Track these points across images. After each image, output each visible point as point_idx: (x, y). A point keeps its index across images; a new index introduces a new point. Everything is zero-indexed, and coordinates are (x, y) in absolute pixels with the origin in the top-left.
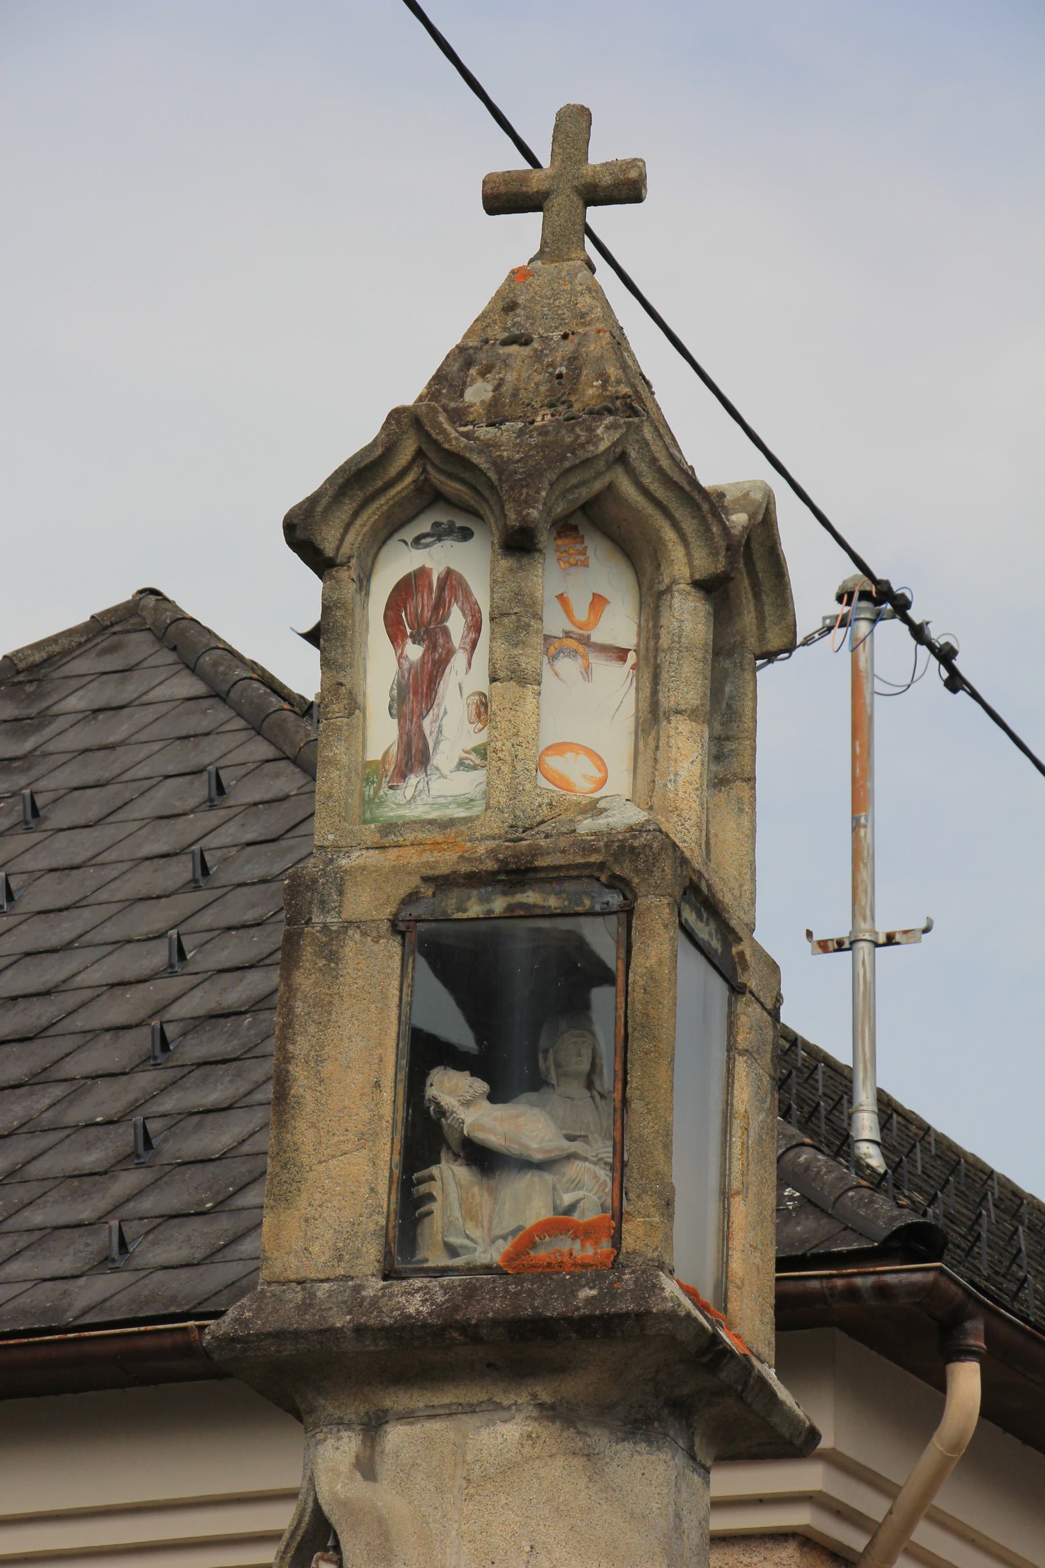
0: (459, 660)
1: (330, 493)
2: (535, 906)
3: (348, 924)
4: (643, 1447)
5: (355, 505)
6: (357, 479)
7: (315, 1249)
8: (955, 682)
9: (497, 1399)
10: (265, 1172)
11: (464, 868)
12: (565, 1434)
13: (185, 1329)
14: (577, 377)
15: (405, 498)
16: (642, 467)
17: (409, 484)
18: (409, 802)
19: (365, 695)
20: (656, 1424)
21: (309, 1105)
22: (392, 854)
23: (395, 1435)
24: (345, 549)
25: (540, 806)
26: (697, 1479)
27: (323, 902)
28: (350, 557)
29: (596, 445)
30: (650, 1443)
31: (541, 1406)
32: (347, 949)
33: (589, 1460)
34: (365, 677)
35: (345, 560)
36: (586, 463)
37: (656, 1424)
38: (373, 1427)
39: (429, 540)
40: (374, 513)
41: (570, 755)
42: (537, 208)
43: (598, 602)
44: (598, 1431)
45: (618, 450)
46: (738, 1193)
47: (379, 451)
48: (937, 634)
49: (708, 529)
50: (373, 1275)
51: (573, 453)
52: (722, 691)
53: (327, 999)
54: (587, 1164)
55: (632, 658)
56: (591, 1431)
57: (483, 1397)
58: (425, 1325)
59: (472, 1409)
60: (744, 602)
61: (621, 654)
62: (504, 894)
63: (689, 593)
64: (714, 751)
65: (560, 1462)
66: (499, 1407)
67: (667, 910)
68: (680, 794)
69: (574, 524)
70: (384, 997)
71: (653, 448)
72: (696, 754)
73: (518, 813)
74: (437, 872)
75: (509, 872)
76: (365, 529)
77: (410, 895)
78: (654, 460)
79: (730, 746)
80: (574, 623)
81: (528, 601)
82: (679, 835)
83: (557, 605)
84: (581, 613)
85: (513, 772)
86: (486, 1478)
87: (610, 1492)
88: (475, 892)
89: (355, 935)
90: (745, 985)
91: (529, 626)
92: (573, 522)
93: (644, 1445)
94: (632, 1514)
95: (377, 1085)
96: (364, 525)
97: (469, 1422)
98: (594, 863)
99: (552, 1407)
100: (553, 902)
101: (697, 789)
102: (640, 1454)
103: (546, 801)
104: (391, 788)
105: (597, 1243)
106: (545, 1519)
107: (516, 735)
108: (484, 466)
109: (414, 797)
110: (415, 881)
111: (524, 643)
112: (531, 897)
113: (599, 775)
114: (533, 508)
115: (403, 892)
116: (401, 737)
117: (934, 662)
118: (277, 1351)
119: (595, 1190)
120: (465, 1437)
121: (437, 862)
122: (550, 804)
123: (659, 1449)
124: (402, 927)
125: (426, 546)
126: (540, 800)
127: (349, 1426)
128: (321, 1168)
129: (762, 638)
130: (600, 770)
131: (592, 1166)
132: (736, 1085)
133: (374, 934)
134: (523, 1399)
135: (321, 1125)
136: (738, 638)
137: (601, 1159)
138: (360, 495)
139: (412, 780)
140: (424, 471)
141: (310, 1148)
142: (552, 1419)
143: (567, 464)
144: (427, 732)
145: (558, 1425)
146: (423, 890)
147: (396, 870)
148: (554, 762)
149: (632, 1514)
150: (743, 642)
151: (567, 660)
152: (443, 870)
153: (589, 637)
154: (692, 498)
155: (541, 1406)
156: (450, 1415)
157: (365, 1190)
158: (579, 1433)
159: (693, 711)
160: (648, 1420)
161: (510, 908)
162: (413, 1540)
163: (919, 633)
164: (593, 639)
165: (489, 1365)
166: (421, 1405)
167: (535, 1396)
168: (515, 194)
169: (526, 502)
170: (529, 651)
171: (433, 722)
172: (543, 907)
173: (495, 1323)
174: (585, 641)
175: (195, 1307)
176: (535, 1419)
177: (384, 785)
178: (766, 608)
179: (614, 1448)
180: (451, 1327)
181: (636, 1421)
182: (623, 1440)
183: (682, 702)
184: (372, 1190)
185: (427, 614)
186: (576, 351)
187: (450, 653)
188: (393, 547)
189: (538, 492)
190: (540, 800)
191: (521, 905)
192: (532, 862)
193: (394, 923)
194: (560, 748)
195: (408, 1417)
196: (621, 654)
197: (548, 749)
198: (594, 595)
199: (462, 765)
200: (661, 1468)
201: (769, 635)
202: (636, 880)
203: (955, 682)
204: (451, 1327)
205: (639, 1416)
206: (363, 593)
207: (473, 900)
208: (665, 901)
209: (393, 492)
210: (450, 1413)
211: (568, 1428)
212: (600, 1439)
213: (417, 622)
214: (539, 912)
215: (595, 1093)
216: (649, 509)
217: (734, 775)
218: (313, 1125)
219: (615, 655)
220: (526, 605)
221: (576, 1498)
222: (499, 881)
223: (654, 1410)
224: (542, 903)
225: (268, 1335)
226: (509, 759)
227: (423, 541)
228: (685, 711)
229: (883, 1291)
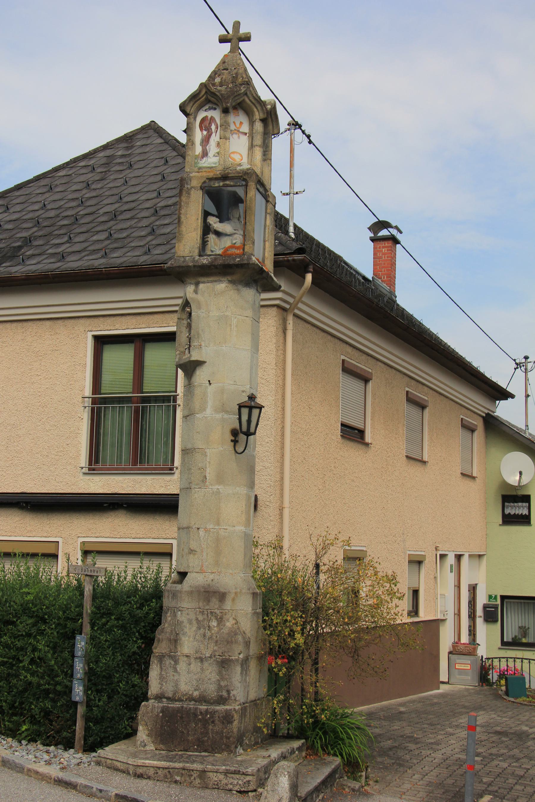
0: (214, 134)
6: (194, 97)
7: (186, 250)
8: (310, 142)
11: (214, 177)
16: (250, 96)
22: (200, 173)
23: (201, 286)
26: (258, 294)
36: (239, 95)
38: (197, 284)
42: (229, 42)
43: (241, 123)
47: (198, 92)
48: (307, 132)
55: (248, 134)
59: (216, 281)
61: (246, 134)
66: (221, 281)
70: (199, 202)
84: (238, 125)
97: (215, 283)
100: (232, 183)
110: (205, 179)
112: (228, 182)
115: (203, 181)
117: (306, 138)
127: (192, 284)
129: (273, 131)
138: (194, 101)
139: (204, 159)
142: (231, 283)
148: (232, 155)
152: (211, 177)
155: (229, 281)
161: (224, 184)
163: (303, 132)
174: (239, 131)
187: (212, 133)
193: (201, 187)
196: (246, 134)
199: (214, 156)
203: (310, 142)
210: (212, 282)
212: (240, 287)
213: (206, 127)
216: (251, 104)
229: (294, 260)
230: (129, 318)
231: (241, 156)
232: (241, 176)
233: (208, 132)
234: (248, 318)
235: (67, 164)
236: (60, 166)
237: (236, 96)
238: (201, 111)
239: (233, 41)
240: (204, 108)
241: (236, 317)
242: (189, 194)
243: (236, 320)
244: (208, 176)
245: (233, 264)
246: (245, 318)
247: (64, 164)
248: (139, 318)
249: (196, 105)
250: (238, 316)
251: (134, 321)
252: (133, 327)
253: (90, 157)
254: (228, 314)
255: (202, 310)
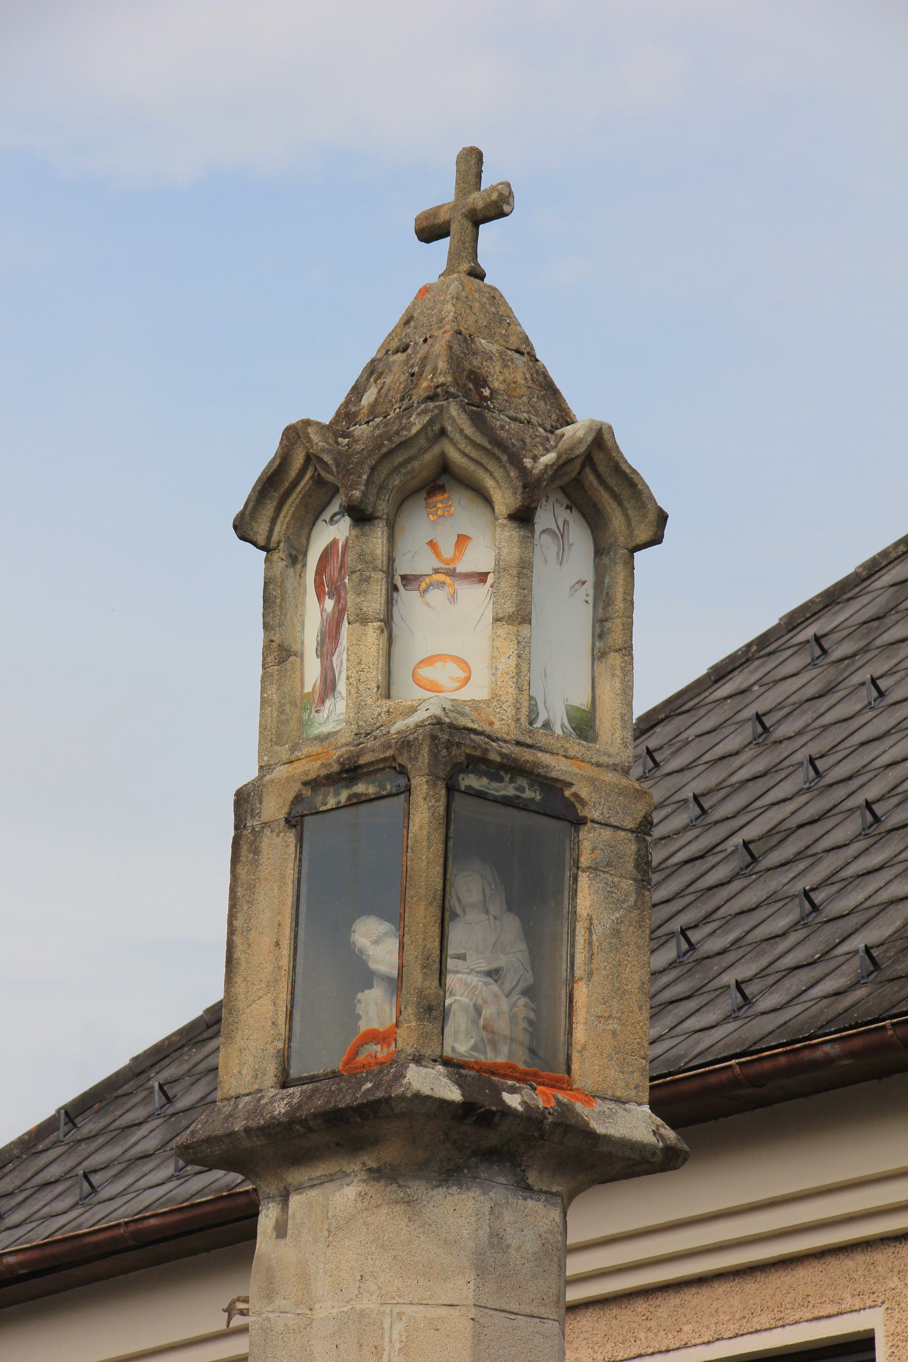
1: (254, 499)
2: (362, 794)
3: (265, 825)
4: (454, 1189)
5: (275, 503)
6: (271, 485)
7: (244, 1072)
9: (344, 1169)
10: (221, 1020)
11: (323, 772)
12: (388, 1189)
13: (730, 1067)
14: (421, 375)
15: (309, 490)
16: (457, 437)
17: (308, 481)
18: (325, 721)
19: (302, 643)
20: (466, 1171)
21: (243, 965)
23: (295, 1201)
24: (275, 538)
25: (379, 714)
27: (252, 810)
28: (279, 542)
29: (409, 430)
30: (460, 1185)
31: (370, 1170)
32: (263, 844)
33: (409, 1205)
34: (303, 629)
35: (275, 545)
36: (402, 445)
37: (466, 1171)
39: (338, 517)
40: (291, 506)
41: (439, 665)
42: (447, 234)
43: (462, 540)
44: (417, 1183)
45: (437, 427)
46: (581, 979)
47: (277, 462)
49: (509, 475)
50: (272, 1087)
51: (389, 440)
52: (603, 582)
53: (253, 883)
54: (459, 975)
55: (491, 579)
56: (410, 1184)
57: (337, 1169)
58: (279, 1123)
59: (331, 1178)
60: (610, 511)
61: (482, 577)
62: (347, 787)
63: (505, 526)
64: (598, 630)
65: (384, 1210)
67: (426, 787)
68: (499, 683)
69: (441, 483)
70: (283, 877)
71: (458, 421)
72: (512, 650)
73: (361, 723)
74: (309, 778)
75: (347, 771)
76: (287, 519)
77: (296, 797)
78: (462, 431)
79: (608, 625)
80: (443, 561)
81: (369, 558)
82: (498, 716)
83: (428, 549)
84: (448, 551)
85: (357, 693)
86: (339, 1228)
87: (427, 1227)
88: (332, 789)
89: (267, 832)
90: (586, 817)
91: (370, 577)
92: (440, 482)
93: (455, 1188)
94: (445, 1241)
95: (277, 944)
96: (285, 517)
97: (330, 1187)
98: (389, 757)
99: (378, 1170)
100: (371, 790)
101: (513, 677)
102: (452, 1195)
103: (385, 709)
104: (317, 711)
105: (389, 1046)
106: (373, 1254)
107: (360, 663)
108: (330, 462)
109: (328, 717)
110: (297, 786)
111: (365, 592)
112: (360, 788)
113: (463, 675)
114: (356, 489)
115: (291, 796)
116: (322, 672)
118: (212, 1152)
119: (466, 994)
120: (328, 1199)
121: (309, 770)
122: (388, 712)
123: (468, 1189)
124: (293, 822)
125: (337, 522)
126: (379, 710)
128: (248, 1011)
129: (631, 535)
130: (464, 671)
131: (464, 976)
132: (580, 895)
133: (277, 830)
134: (357, 1167)
135: (249, 979)
136: (613, 539)
137: (472, 970)
138: (277, 495)
139: (328, 703)
140: (316, 469)
141: (243, 997)
142: (377, 1179)
143: (384, 450)
144: (335, 665)
145: (382, 1182)
146: (304, 792)
147: (288, 779)
148: (426, 673)
149: (445, 1241)
150: (615, 542)
151: (436, 591)
152: (312, 776)
153: (454, 569)
154: (494, 454)
155: (370, 1170)
156: (321, 1184)
157: (269, 1023)
158: (400, 1186)
159: (509, 617)
160: (458, 1169)
161: (349, 798)
162: (293, 1280)
164: (458, 571)
165: (338, 1145)
166: (306, 1178)
167: (364, 1164)
168: (433, 226)
169: (351, 486)
170: (370, 597)
171: (338, 657)
172: (365, 795)
173: (315, 1116)
174: (452, 573)
175: (751, 1047)
176: (364, 1181)
177: (313, 710)
178: (630, 512)
179: (430, 1194)
180: (295, 1122)
181: (448, 1171)
182: (438, 1187)
183: (500, 611)
184: (273, 1023)
185: (336, 575)
186: (428, 352)
188: (320, 525)
189: (360, 477)
190: (379, 710)
191: (355, 795)
192: (356, 762)
193: (287, 821)
194: (430, 661)
195: (299, 1189)
196: (482, 577)
197: (420, 662)
198: (458, 536)
200: (470, 1203)
201: (636, 532)
202: (409, 766)
204: (295, 1122)
205: (450, 1167)
206: (299, 566)
207: (331, 795)
208: (424, 780)
209: (299, 488)
210: (321, 1183)
211: (391, 1184)
212: (418, 1188)
213: (332, 583)
214: (364, 798)
215: (491, 917)
216: (472, 467)
217: (610, 648)
218: (245, 979)
219: (476, 579)
220: (367, 563)
221: (398, 1235)
222: (343, 779)
223: (461, 1161)
224: (365, 792)
225: (203, 1141)
226: (355, 683)
227: (335, 518)
228: (503, 618)
230: (721, 1288)
231: (464, 664)
232: (393, 758)
233: (338, 602)
234: (454, 1312)
235: (763, 641)
236: (733, 657)
237: (391, 452)
238: (320, 524)
239: (454, 228)
240: (327, 515)
241: (400, 1315)
242: (256, 851)
243: (399, 1326)
244: (306, 773)
245: (349, 1108)
246: (443, 1311)
247: (749, 646)
248: (750, 1286)
249: (289, 509)
250: (409, 1310)
251: (736, 1302)
252: (733, 1328)
253: (850, 595)
254: (369, 1303)
255: (280, 1302)
